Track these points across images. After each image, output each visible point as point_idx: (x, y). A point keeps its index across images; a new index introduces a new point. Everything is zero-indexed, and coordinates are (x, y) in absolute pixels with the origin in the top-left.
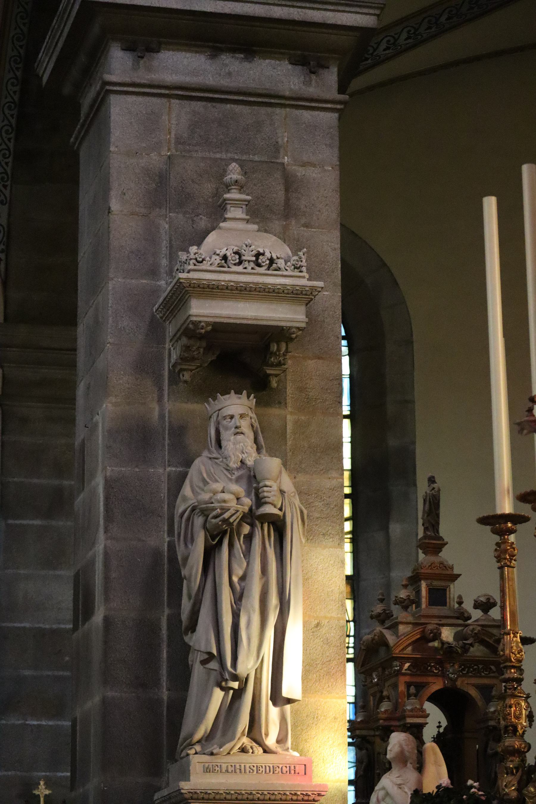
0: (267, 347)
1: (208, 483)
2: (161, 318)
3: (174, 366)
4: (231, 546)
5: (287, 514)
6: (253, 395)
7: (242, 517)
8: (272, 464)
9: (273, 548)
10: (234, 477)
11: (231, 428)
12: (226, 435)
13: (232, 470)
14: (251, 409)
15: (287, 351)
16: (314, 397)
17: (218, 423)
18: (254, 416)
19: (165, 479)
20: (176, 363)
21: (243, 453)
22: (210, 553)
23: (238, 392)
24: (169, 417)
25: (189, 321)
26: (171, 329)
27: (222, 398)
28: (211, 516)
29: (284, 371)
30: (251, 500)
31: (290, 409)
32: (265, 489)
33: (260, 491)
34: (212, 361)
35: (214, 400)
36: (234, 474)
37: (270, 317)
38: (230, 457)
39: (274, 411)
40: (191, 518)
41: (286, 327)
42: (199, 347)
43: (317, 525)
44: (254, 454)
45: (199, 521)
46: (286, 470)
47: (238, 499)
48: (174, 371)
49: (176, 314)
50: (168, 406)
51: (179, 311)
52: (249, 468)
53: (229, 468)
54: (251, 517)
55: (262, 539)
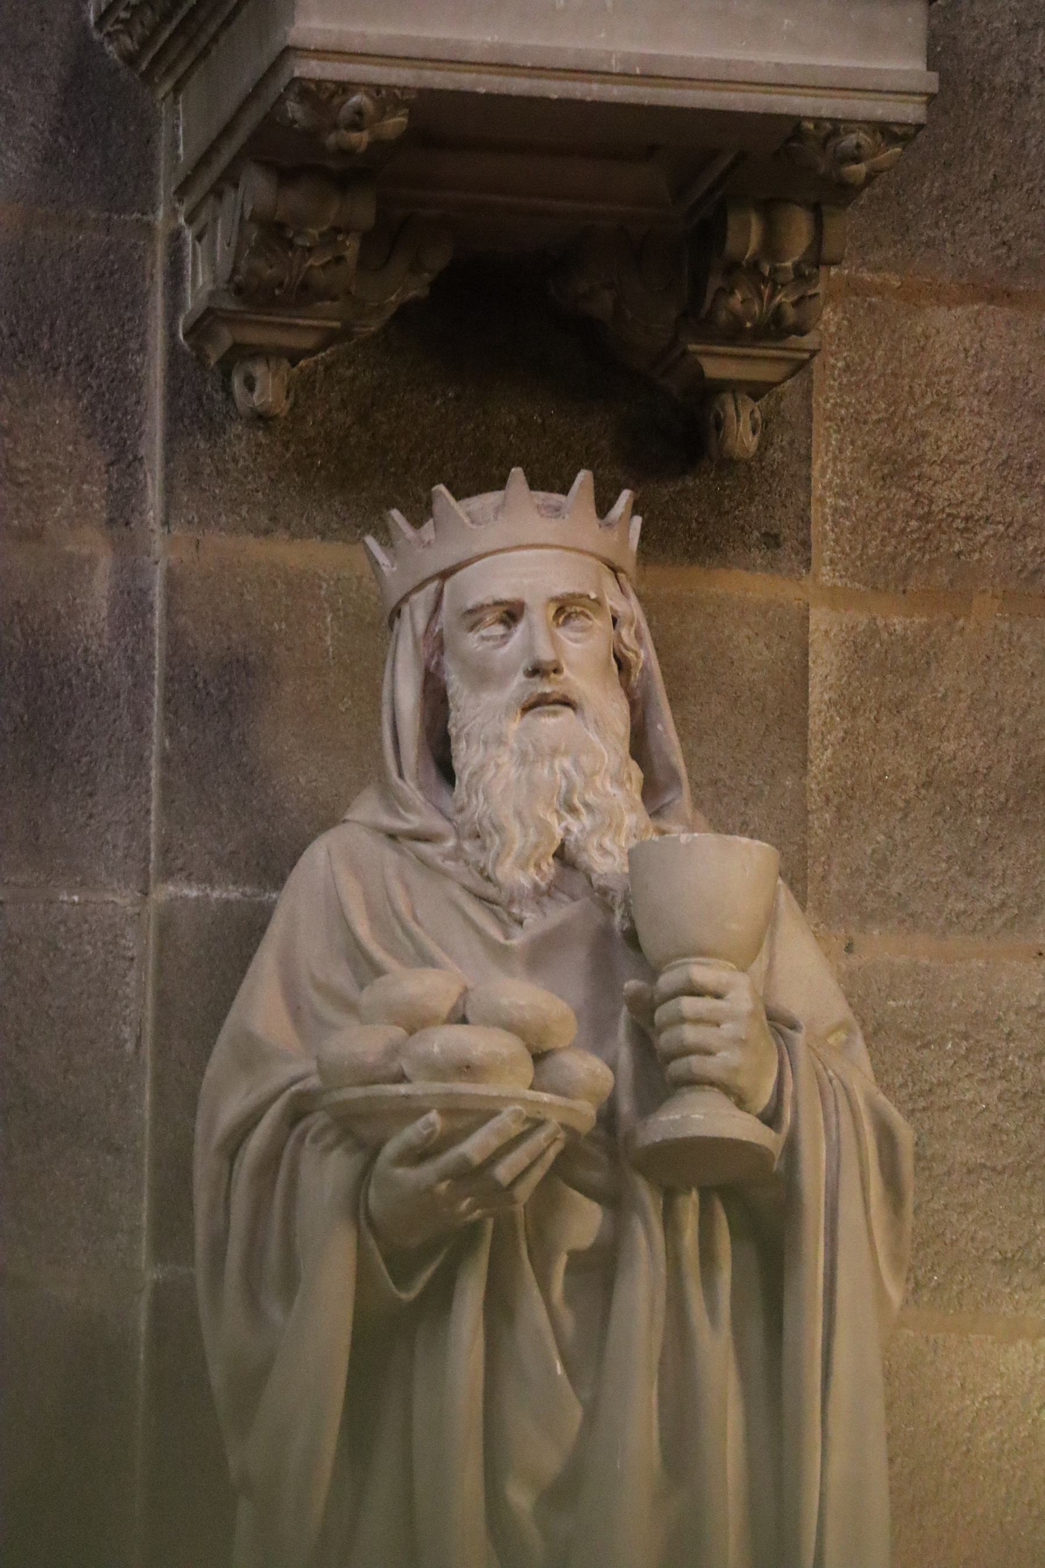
0: (709, 234)
1: (378, 971)
2: (131, 60)
3: (201, 329)
4: (499, 1307)
5: (805, 1150)
6: (625, 497)
7: (562, 1154)
8: (723, 873)
9: (726, 1330)
10: (519, 939)
11: (501, 679)
12: (483, 717)
13: (511, 901)
14: (615, 570)
15: (817, 258)
16: (963, 511)
17: (436, 645)
18: (630, 607)
19: (140, 943)
20: (209, 311)
21: (572, 810)
22: (388, 1343)
23: (551, 479)
24: (170, 613)
25: (284, 80)
26: (180, 129)
27: (460, 508)
28: (391, 1149)
29: (801, 366)
30: (613, 1067)
31: (826, 575)
32: (688, 1005)
33: (661, 1015)
34: (403, 313)
35: (417, 523)
36: (520, 923)
37: (729, 64)
38: (499, 829)
39: (744, 586)
40: (285, 1162)
41: (818, 121)
42: (336, 230)
43: (966, 1208)
44: (633, 818)
45: (325, 1174)
46: (802, 899)
47: (539, 1057)
48: (201, 359)
49: (215, 39)
50: (163, 547)
51: (227, 23)
52: (604, 891)
53: (491, 891)
54: (608, 1156)
55: (669, 1279)
